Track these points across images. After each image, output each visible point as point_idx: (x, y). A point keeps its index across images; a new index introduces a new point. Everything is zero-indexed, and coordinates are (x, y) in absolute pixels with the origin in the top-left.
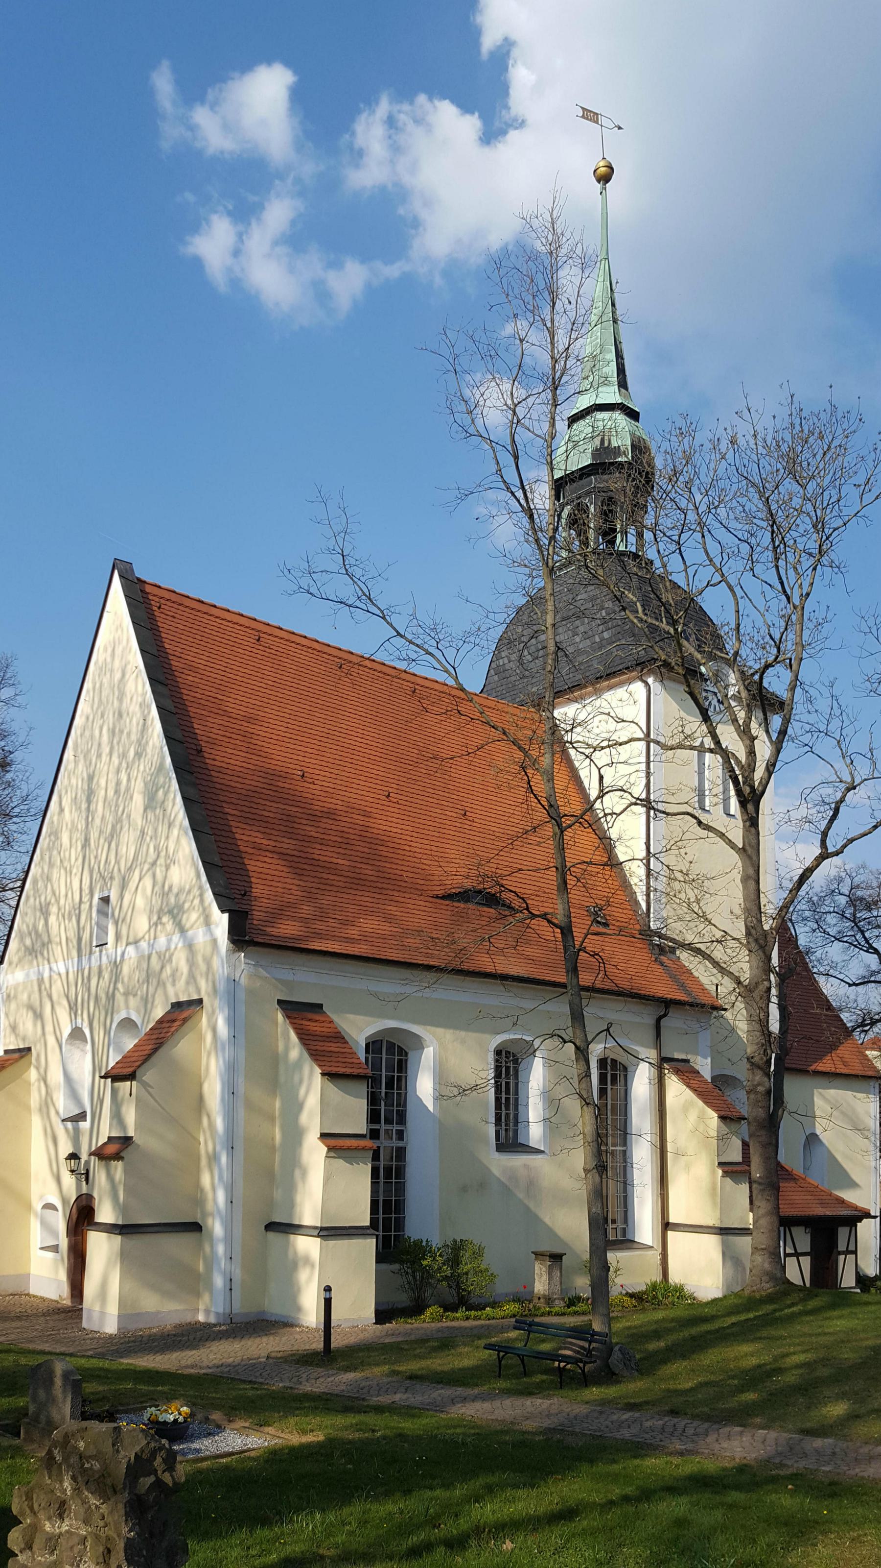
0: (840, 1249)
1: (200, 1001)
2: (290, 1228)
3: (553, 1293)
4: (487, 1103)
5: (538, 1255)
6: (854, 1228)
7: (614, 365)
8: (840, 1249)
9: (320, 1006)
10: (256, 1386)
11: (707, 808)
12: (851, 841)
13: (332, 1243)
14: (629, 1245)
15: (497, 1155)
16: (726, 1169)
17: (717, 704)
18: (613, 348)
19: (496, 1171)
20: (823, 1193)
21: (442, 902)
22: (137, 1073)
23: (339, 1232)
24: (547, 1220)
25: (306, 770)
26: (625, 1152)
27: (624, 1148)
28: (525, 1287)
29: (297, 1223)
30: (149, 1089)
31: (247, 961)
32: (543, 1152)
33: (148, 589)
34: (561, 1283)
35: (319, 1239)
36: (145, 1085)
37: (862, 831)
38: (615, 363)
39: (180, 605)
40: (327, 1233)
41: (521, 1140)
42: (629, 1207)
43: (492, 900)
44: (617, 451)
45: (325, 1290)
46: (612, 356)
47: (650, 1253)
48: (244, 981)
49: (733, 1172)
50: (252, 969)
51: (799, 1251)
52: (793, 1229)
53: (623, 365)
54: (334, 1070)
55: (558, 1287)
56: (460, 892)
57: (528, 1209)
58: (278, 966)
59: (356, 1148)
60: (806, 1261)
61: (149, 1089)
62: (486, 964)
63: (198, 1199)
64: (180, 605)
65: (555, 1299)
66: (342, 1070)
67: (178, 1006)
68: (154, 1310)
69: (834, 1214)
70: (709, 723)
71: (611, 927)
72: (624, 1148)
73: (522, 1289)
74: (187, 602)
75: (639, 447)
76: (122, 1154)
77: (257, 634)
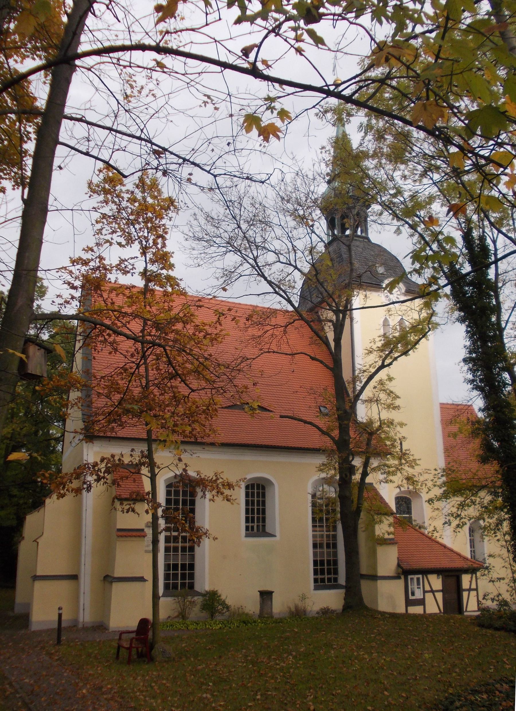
60: (439, 596)
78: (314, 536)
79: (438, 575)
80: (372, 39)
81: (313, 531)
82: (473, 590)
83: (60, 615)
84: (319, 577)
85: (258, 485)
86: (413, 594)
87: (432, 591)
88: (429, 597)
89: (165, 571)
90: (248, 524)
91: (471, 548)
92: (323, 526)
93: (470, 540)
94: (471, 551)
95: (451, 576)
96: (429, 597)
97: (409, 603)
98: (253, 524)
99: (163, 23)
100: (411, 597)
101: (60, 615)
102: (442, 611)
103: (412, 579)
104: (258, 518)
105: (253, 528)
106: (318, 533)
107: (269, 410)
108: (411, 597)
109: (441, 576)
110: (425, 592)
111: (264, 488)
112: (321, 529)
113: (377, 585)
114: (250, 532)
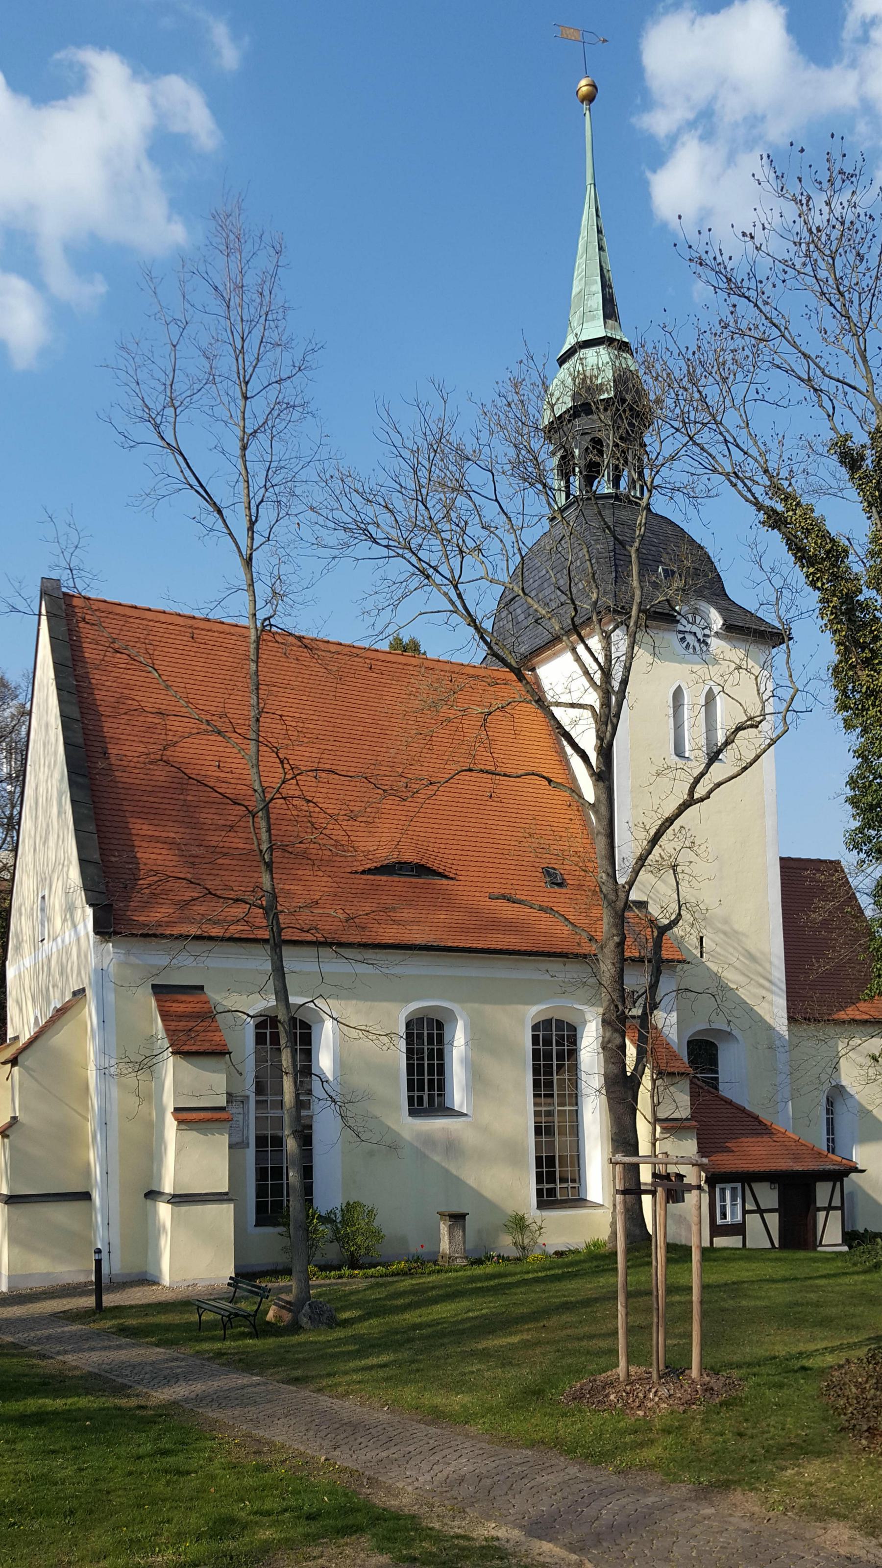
0: (819, 1205)
1: (83, 990)
2: (153, 1195)
3: (455, 1252)
4: (399, 1069)
5: (442, 1214)
6: (838, 1184)
7: (599, 297)
8: (819, 1205)
9: (201, 988)
10: (170, 1336)
11: (687, 755)
12: (718, 785)
13: (184, 1209)
14: (582, 1203)
15: (410, 1119)
16: (665, 1125)
17: (697, 645)
18: (599, 278)
19: (406, 1135)
20: (803, 1147)
21: (362, 876)
22: (19, 1059)
23: (185, 1199)
24: (471, 1182)
25: (222, 759)
26: (577, 1111)
27: (575, 1108)
28: (422, 1246)
29: (157, 1189)
30: (32, 1073)
31: (116, 950)
32: (466, 1115)
33: (76, 602)
34: (464, 1243)
35: (170, 1206)
36: (27, 1069)
37: (730, 774)
38: (600, 295)
39: (110, 613)
40: (179, 1199)
41: (448, 1105)
42: (582, 1166)
43: (422, 870)
44: (600, 389)
45: (95, 1253)
46: (598, 287)
47: (600, 1211)
48: (112, 970)
49: (672, 1128)
50: (122, 957)
51: (762, 1208)
52: (756, 1186)
53: (611, 295)
54: (186, 1048)
55: (461, 1246)
56: (376, 867)
57: (447, 1171)
58: (153, 952)
59: (209, 1120)
60: (773, 1220)
61: (32, 1073)
62: (390, 934)
63: (87, 1172)
64: (110, 613)
65: (457, 1258)
66: (194, 1048)
67: (75, 994)
68: (45, 1271)
69: (821, 1168)
70: (524, 682)
71: (487, 894)
72: (575, 1108)
73: (420, 1250)
74: (119, 610)
75: (623, 379)
76: (7, 1133)
77: (190, 630)
78: (537, 1114)
79: (772, 1183)
80: (745, 711)
81: (535, 1104)
82: (836, 1208)
83: (98, 1263)
84: (546, 1186)
85: (430, 1021)
86: (724, 1216)
87: (760, 1211)
88: (753, 1220)
89: (257, 1180)
90: (411, 1094)
91: (828, 1134)
92: (552, 1096)
93: (828, 1119)
94: (828, 1139)
95: (689, 1128)
96: (753, 1220)
97: (716, 1230)
98: (420, 1094)
99: (733, 1032)
100: (719, 1222)
101: (98, 1263)
102: (777, 1246)
103: (723, 1191)
104: (431, 1082)
105: (420, 1098)
106: (543, 1109)
107: (446, 877)
108: (719, 1222)
109: (777, 1185)
110: (745, 1212)
111: (440, 1025)
112: (549, 1100)
113: (155, 1206)
114: (417, 1108)
